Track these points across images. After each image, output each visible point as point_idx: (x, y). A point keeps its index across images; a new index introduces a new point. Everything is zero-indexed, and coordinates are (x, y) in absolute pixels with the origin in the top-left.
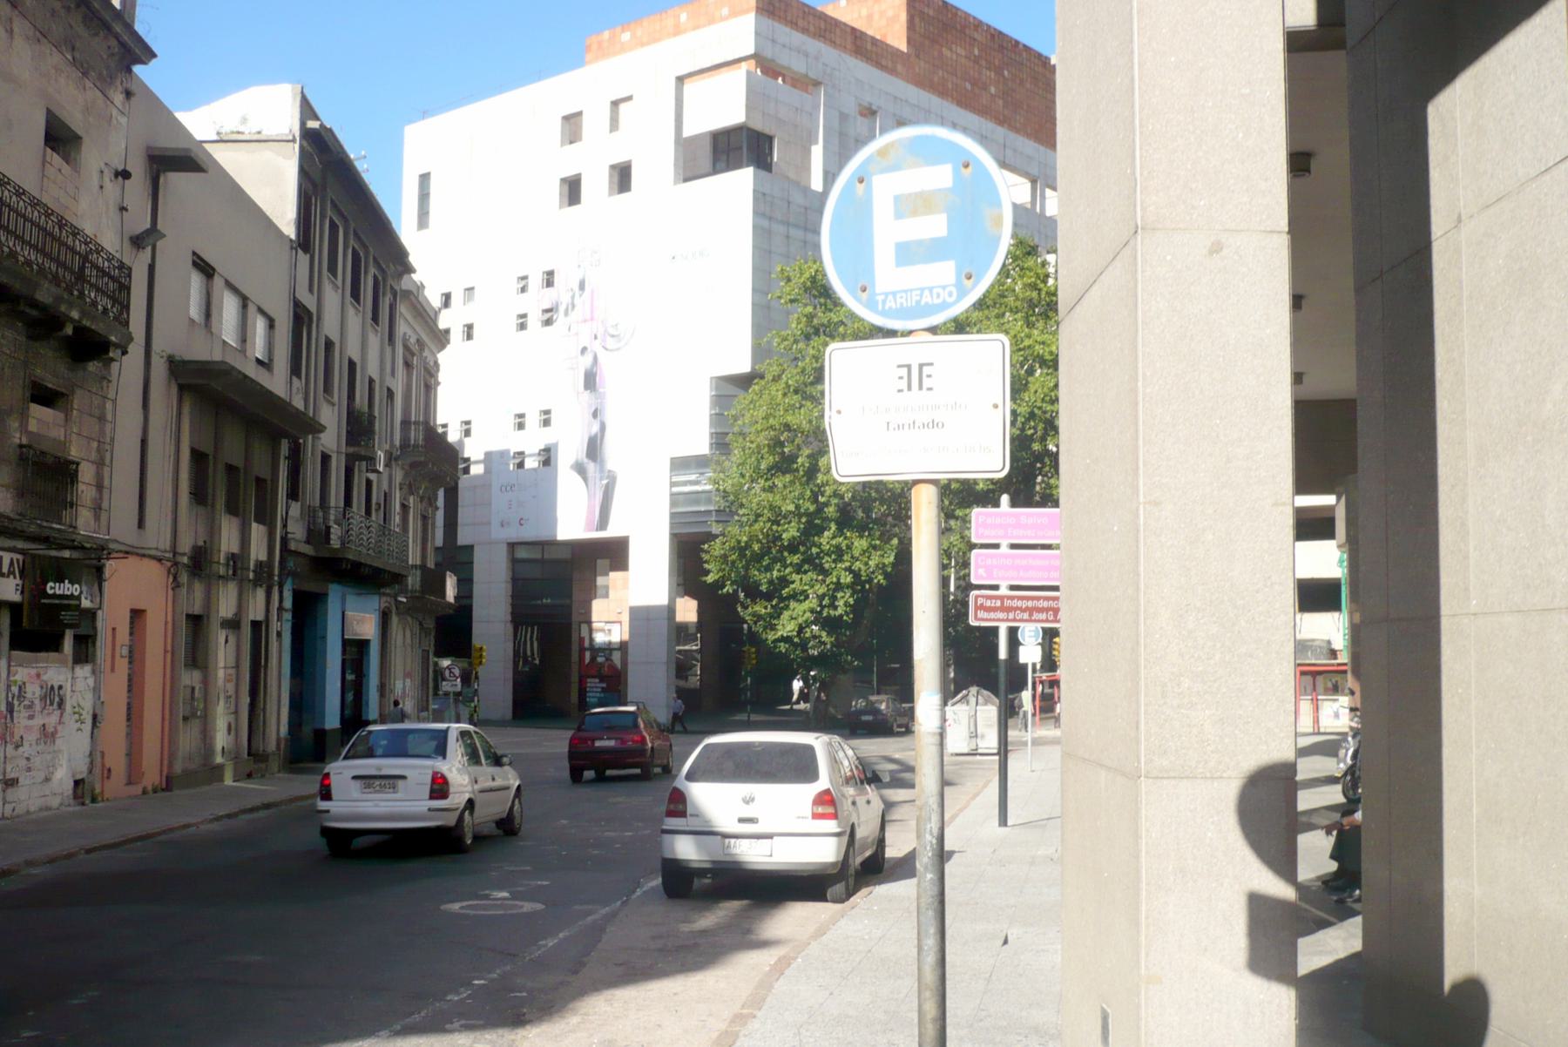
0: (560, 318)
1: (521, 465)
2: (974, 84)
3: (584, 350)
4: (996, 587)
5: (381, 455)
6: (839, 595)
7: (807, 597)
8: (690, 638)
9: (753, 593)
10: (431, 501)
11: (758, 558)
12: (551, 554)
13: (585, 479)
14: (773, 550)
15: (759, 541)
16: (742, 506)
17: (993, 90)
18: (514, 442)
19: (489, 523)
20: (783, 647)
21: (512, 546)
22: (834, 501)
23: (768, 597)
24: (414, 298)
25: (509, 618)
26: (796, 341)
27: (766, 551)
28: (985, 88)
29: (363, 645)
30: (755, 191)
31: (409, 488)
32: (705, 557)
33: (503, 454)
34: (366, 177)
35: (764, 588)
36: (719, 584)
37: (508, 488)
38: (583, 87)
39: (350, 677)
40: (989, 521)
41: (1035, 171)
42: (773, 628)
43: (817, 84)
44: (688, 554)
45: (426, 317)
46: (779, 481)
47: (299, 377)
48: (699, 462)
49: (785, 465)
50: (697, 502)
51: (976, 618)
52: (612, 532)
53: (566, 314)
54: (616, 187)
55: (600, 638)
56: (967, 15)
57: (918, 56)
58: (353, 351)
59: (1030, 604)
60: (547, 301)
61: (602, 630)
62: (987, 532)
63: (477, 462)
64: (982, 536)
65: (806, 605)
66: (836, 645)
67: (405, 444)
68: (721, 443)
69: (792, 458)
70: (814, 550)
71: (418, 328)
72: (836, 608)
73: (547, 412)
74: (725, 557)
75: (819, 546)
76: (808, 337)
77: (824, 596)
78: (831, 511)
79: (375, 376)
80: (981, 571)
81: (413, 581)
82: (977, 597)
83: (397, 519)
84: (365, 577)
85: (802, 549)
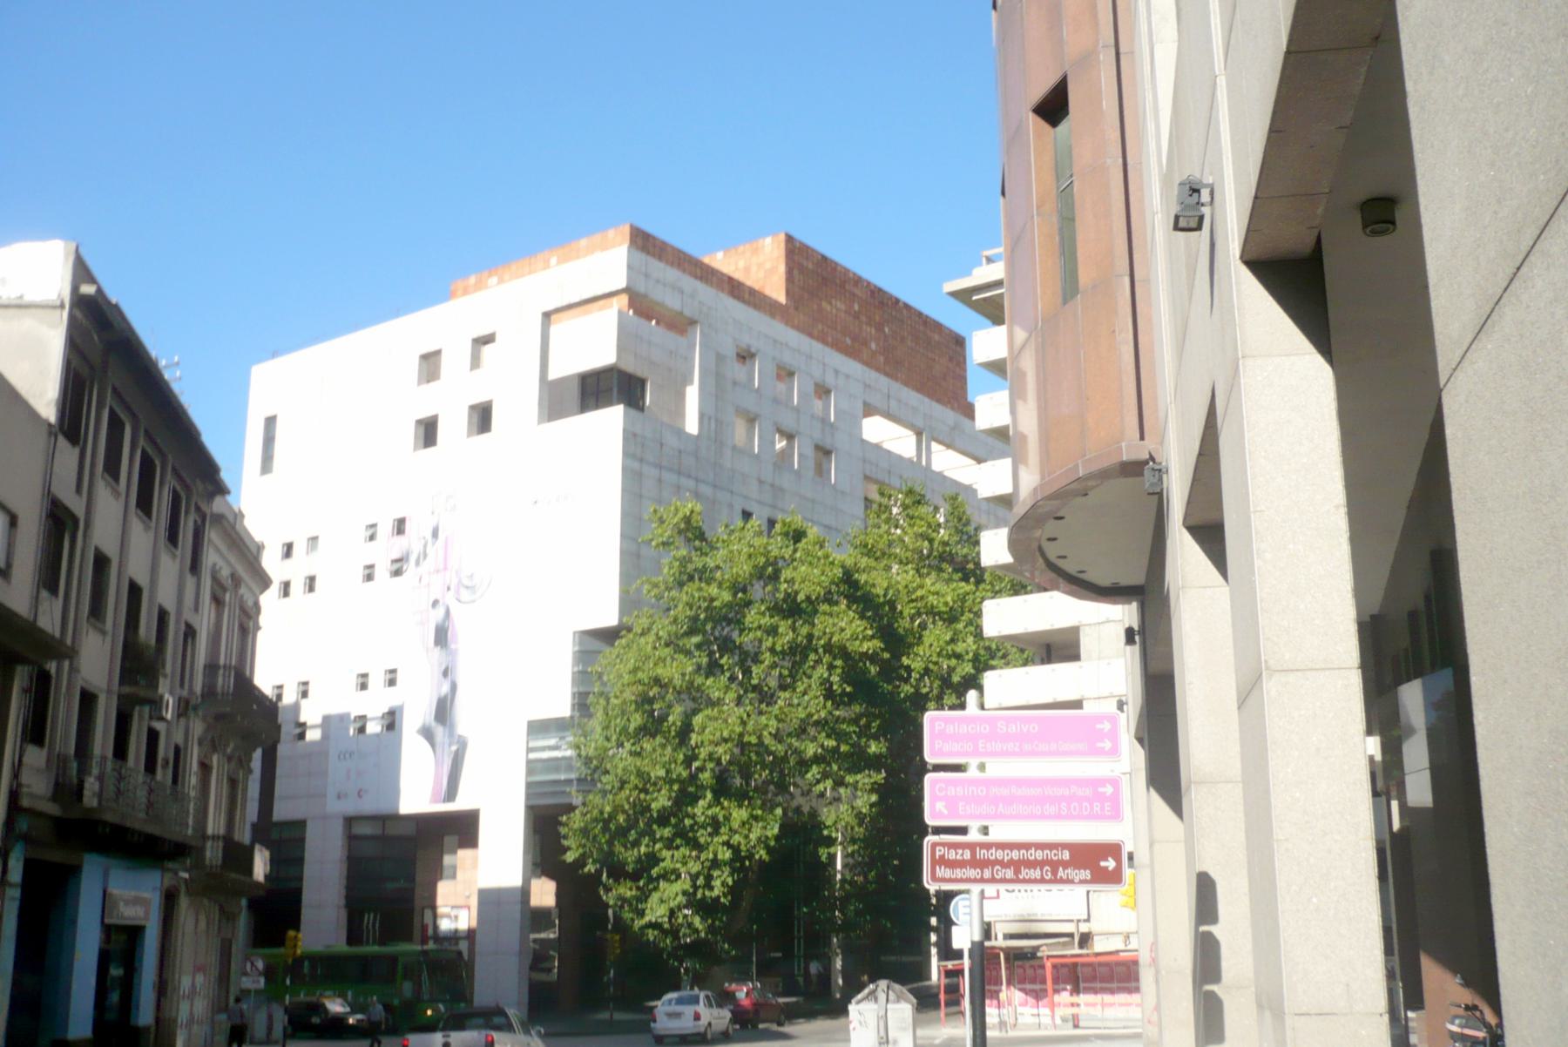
0: (410, 568)
1: (362, 730)
2: (854, 339)
3: (435, 603)
4: (963, 831)
5: (170, 700)
6: (716, 873)
7: (679, 876)
8: (549, 925)
9: (618, 872)
10: (244, 762)
11: (622, 832)
12: (394, 830)
13: (433, 745)
14: (641, 819)
15: (624, 812)
16: (607, 772)
17: (873, 346)
18: (354, 704)
19: (325, 796)
20: (651, 935)
21: (350, 821)
22: (710, 765)
23: (635, 877)
24: (232, 530)
25: (343, 902)
26: (669, 589)
27: (631, 824)
28: (865, 343)
29: (134, 933)
30: (625, 431)
31: (212, 744)
32: (563, 830)
33: (343, 718)
34: (176, 387)
35: (630, 868)
36: (580, 862)
37: (346, 755)
38: (444, 324)
39: (116, 972)
40: (950, 729)
41: (920, 423)
42: (641, 914)
43: (693, 322)
44: (545, 825)
45: (247, 553)
46: (647, 745)
47: (54, 590)
48: (558, 725)
49: (653, 727)
50: (557, 770)
51: (934, 878)
52: (460, 804)
53: (417, 563)
54: (475, 428)
55: (445, 925)
56: (847, 271)
57: (797, 309)
58: (137, 569)
59: (1015, 855)
60: (398, 548)
61: (448, 916)
62: (946, 748)
63: (314, 727)
64: (941, 753)
65: (678, 887)
66: (711, 929)
67: (209, 692)
68: (582, 704)
69: (663, 718)
70: (688, 822)
71: (233, 560)
72: (711, 888)
73: (393, 671)
74: (585, 832)
75: (693, 817)
76: (681, 584)
77: (697, 875)
78: (705, 777)
79: (170, 606)
80: (940, 806)
81: (213, 854)
82: (934, 845)
83: (194, 780)
84: (144, 849)
85: (673, 821)
